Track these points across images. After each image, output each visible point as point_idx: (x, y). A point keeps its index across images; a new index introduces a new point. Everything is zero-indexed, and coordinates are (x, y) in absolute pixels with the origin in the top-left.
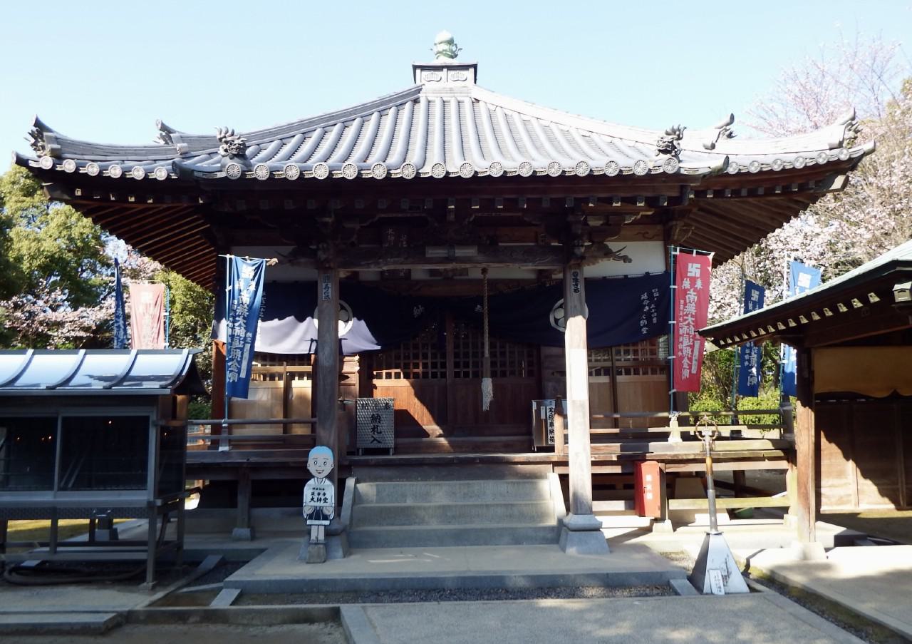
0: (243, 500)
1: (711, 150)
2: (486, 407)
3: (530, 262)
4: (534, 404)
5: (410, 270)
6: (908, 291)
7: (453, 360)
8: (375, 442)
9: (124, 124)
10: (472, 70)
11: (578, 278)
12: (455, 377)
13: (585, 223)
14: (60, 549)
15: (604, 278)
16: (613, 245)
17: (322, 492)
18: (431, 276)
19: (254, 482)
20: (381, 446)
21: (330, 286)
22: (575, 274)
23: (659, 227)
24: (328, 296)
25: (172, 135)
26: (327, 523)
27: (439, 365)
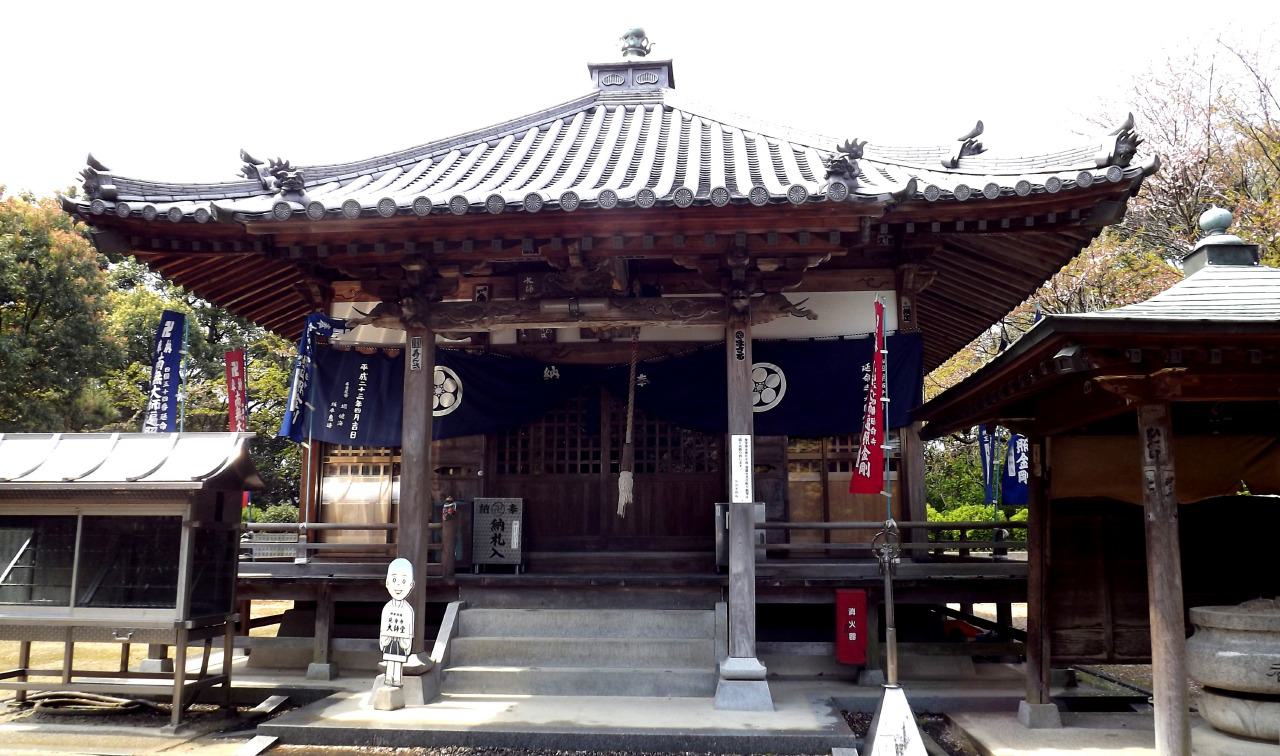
0: (321, 629)
1: (953, 168)
2: (620, 511)
3: (680, 319)
4: (718, 508)
5: (554, 330)
6: (1071, 360)
7: (608, 449)
8: (496, 556)
9: (188, 159)
10: (665, 69)
11: (743, 339)
12: (612, 471)
13: (754, 268)
14: (74, 679)
15: (812, 339)
16: (792, 297)
17: (399, 618)
18: (582, 336)
19: (338, 605)
20: (503, 561)
21: (420, 351)
22: (740, 335)
23: (889, 272)
24: (417, 365)
25: (257, 166)
26: (403, 659)
27: (591, 456)
